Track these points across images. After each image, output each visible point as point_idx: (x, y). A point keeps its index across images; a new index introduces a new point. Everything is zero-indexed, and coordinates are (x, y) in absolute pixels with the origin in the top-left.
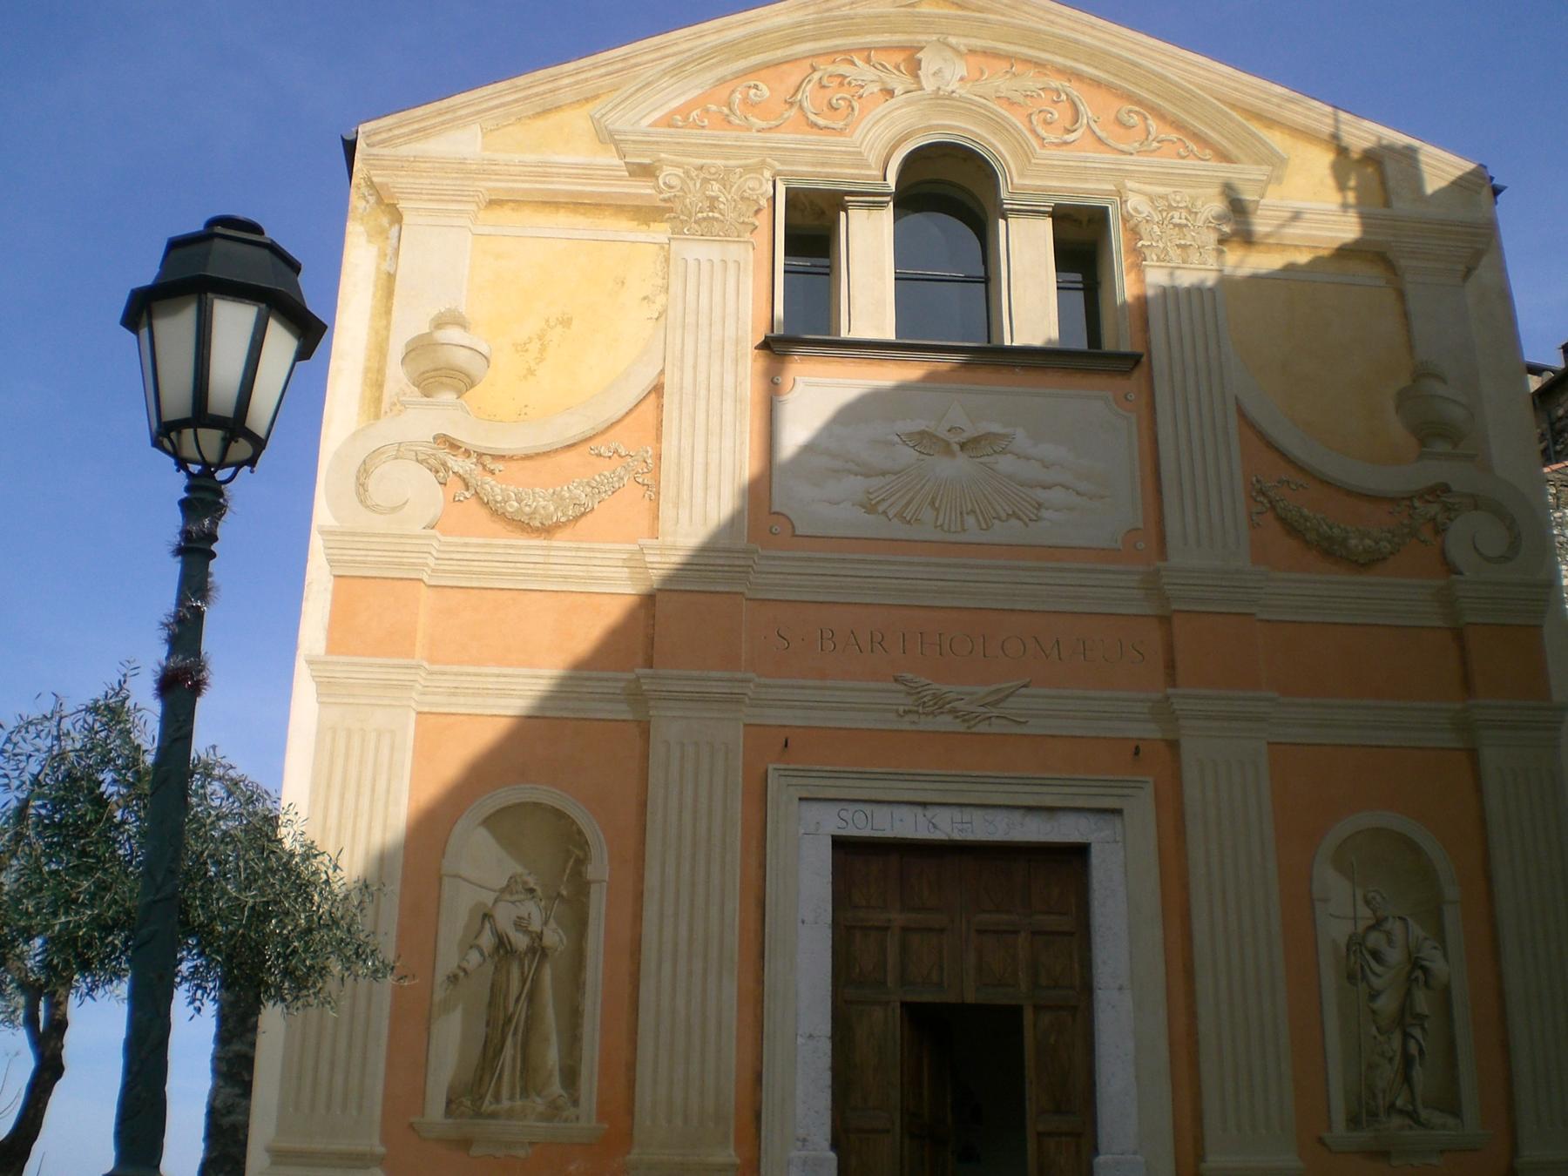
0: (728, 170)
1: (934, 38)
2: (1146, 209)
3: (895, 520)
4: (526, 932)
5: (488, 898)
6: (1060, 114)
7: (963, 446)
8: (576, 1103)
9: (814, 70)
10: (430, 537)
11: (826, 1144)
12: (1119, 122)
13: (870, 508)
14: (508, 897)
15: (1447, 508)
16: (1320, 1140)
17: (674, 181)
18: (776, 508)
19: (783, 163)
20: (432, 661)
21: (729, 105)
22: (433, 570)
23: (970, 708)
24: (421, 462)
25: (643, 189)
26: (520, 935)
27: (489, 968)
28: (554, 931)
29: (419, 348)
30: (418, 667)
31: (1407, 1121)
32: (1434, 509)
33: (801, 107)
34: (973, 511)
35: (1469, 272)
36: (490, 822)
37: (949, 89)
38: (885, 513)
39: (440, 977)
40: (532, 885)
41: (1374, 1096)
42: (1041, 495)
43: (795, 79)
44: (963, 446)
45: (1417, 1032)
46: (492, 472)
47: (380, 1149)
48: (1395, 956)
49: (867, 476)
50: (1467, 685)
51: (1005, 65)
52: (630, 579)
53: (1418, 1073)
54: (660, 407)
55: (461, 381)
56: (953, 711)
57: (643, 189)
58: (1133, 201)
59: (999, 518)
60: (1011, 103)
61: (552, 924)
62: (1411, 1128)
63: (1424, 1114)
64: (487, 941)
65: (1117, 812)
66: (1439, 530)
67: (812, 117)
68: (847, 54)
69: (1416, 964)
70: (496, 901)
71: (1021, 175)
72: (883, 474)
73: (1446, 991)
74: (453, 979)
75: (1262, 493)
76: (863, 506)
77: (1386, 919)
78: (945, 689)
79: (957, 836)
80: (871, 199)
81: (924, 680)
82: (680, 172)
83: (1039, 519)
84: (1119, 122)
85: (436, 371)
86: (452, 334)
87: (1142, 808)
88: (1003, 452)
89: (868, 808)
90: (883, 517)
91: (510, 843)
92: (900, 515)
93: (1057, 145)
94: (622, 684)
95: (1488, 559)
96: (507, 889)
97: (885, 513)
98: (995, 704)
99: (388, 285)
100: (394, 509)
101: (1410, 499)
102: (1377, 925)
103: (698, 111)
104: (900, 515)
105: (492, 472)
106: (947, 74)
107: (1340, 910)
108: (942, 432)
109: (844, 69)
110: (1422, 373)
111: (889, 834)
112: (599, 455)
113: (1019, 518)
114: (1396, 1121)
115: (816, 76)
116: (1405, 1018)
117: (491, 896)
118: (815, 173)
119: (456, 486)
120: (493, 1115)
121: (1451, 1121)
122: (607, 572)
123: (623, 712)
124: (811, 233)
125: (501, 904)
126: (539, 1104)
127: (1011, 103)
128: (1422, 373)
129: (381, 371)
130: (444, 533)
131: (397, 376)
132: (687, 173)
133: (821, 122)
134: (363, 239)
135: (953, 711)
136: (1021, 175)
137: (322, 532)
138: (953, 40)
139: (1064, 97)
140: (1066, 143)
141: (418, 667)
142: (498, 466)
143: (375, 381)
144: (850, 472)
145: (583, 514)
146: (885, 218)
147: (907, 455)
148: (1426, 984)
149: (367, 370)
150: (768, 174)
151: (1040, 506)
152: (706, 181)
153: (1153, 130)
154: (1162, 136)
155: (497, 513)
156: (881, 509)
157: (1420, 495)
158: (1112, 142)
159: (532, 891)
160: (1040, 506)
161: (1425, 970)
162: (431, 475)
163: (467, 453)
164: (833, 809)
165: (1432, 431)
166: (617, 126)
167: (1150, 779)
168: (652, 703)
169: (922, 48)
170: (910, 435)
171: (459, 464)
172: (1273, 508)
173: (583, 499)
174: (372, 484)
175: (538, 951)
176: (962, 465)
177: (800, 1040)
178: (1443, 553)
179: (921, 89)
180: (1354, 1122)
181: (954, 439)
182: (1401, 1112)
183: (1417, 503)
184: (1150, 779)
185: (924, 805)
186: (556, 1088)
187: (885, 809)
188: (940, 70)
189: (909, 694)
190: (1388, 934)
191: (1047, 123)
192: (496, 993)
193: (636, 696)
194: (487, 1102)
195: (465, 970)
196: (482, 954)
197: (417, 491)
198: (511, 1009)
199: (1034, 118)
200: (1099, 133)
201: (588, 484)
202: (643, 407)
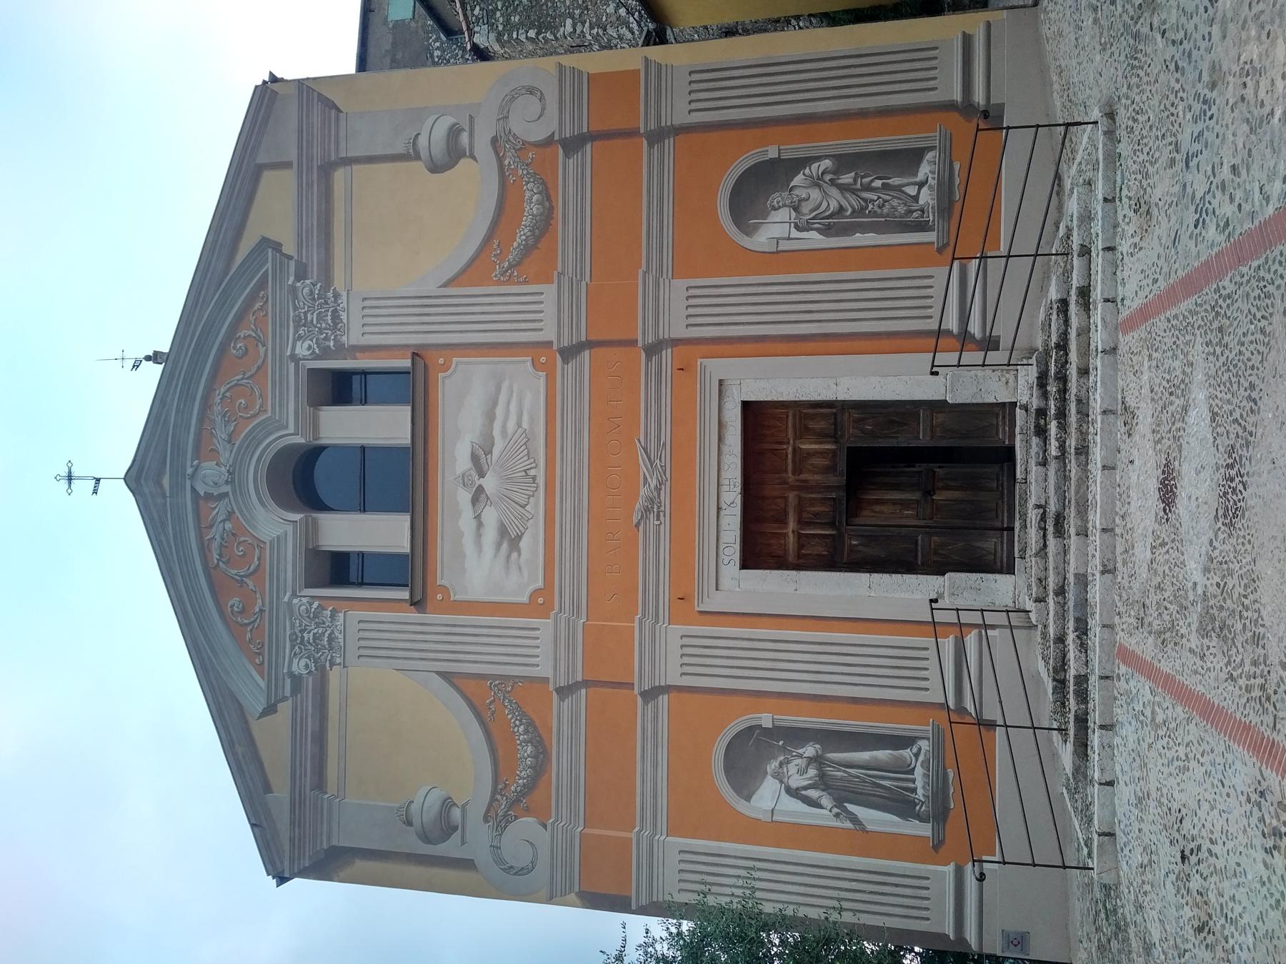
1: (188, 483)
11: (940, 578)
50: (632, 133)
56: (658, 490)
65: (721, 382)
67: (252, 567)
71: (286, 427)
79: (738, 489)
80: (311, 531)
82: (295, 661)
87: (716, 368)
89: (722, 546)
95: (543, 109)
109: (215, 545)
111: (738, 533)
146: (325, 519)
158: (260, 362)
164: (723, 568)
167: (699, 361)
175: (817, 760)
178: (537, 145)
184: (699, 361)
185: (719, 509)
186: (907, 753)
187: (722, 534)
193: (650, 695)
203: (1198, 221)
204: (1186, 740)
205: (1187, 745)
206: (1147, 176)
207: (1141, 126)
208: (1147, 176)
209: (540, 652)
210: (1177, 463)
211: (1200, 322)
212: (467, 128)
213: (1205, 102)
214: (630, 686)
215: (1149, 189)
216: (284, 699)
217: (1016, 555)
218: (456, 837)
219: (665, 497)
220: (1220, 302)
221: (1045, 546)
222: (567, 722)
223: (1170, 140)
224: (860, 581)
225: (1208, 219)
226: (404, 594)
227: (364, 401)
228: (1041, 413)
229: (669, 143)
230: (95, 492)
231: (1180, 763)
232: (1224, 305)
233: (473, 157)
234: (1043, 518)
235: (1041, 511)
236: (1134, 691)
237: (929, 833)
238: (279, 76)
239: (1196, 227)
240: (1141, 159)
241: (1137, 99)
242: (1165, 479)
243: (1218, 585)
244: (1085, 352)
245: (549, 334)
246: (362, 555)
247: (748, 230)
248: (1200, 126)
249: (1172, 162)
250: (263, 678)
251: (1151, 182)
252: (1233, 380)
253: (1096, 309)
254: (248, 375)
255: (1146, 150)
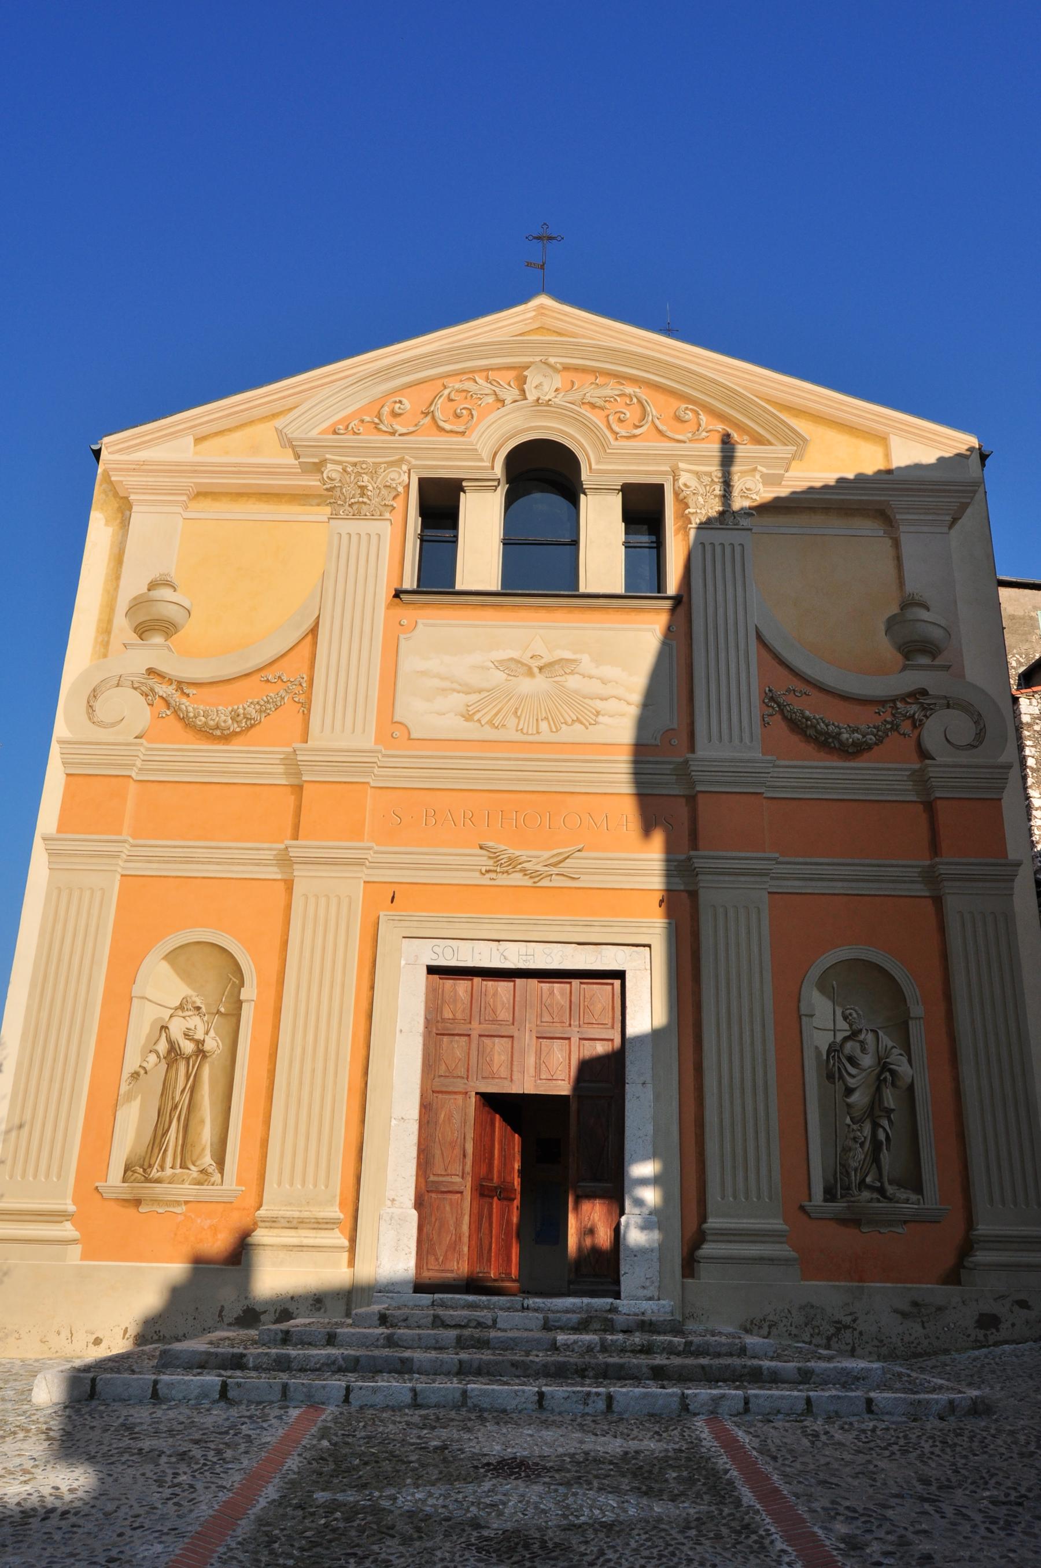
0: (377, 465)
1: (538, 359)
2: (693, 483)
3: (487, 726)
4: (192, 1040)
5: (166, 1014)
6: (631, 414)
7: (541, 669)
8: (221, 1171)
9: (445, 387)
10: (136, 744)
12: (678, 419)
13: (468, 717)
14: (180, 1013)
15: (924, 708)
16: (802, 1208)
17: (334, 475)
18: (395, 720)
19: (415, 458)
20: (134, 838)
21: (379, 416)
22: (140, 769)
23: (539, 867)
24: (135, 689)
25: (312, 482)
26: (188, 1042)
27: (163, 1066)
28: (213, 1039)
29: (138, 604)
30: (125, 841)
31: (875, 1195)
32: (913, 709)
33: (433, 418)
34: (546, 718)
35: (955, 521)
36: (171, 957)
37: (547, 398)
38: (479, 721)
39: (126, 1075)
40: (199, 1004)
41: (848, 1174)
42: (599, 705)
43: (429, 396)
44: (541, 669)
45: (885, 1123)
46: (188, 695)
47: (72, 1208)
48: (867, 1061)
49: (467, 693)
50: (935, 847)
51: (591, 378)
52: (285, 774)
53: (885, 1156)
54: (315, 644)
55: (167, 628)
56: (524, 871)
57: (312, 482)
58: (684, 478)
59: (566, 723)
60: (593, 406)
61: (212, 1033)
62: (879, 1201)
63: (890, 1189)
64: (162, 1047)
66: (917, 724)
67: (442, 424)
68: (470, 373)
69: (884, 1066)
70: (171, 1016)
71: (598, 462)
72: (480, 691)
73: (911, 1088)
74: (135, 1075)
75: (772, 699)
76: (463, 716)
77: (861, 1031)
78: (518, 853)
80: (484, 484)
81: (504, 847)
82: (339, 468)
83: (596, 723)
84: (678, 419)
85: (151, 624)
86: (166, 593)
88: (572, 673)
90: (477, 724)
91: (185, 975)
92: (490, 722)
93: (628, 438)
94: (275, 852)
95: (958, 747)
96: (181, 1007)
97: (479, 721)
98: (555, 865)
99: (118, 559)
100: (113, 725)
101: (894, 701)
102: (854, 1035)
103: (356, 422)
104: (490, 722)
105: (188, 695)
106: (546, 388)
107: (824, 1020)
108: (526, 659)
109: (469, 385)
110: (909, 603)
112: (268, 681)
113: (581, 723)
114: (866, 1195)
115: (446, 392)
116: (875, 1110)
117: (166, 1014)
118: (444, 469)
119: (157, 701)
120: (158, 1181)
121: (914, 1197)
122: (269, 769)
123: (273, 873)
124: (440, 507)
125: (174, 1019)
126: (194, 1172)
127: (593, 406)
128: (909, 603)
129: (110, 621)
130: (150, 741)
131: (121, 623)
132: (345, 470)
133: (447, 426)
134: (103, 522)
135: (524, 871)
136: (598, 462)
137: (59, 742)
138: (552, 360)
139: (635, 400)
140: (635, 436)
141: (125, 841)
142: (190, 691)
143: (106, 629)
144: (454, 690)
145: (252, 726)
147: (499, 676)
148: (893, 1084)
149: (100, 620)
150: (405, 468)
151: (598, 713)
152: (359, 474)
153: (703, 424)
154: (711, 427)
155: (186, 722)
156: (476, 718)
157: (903, 698)
159: (198, 1008)
160: (598, 713)
161: (893, 1072)
162: (142, 699)
163: (170, 681)
165: (916, 648)
166: (295, 435)
168: (296, 866)
169: (528, 368)
170: (501, 662)
171: (163, 689)
172: (781, 711)
173: (254, 714)
174: (97, 705)
175: (201, 1052)
176: (540, 683)
177: (394, 1122)
178: (919, 745)
179: (526, 399)
180: (830, 1194)
181: (535, 664)
182: (870, 1188)
183: (899, 705)
186: (208, 1160)
188: (541, 384)
189: (490, 858)
190: (862, 1043)
191: (620, 421)
192: (166, 1087)
193: (285, 861)
194: (155, 1170)
195: (144, 1068)
196: (158, 1057)
197: (132, 711)
198: (177, 1099)
199: (611, 418)
200: (661, 427)
201: (258, 703)
202: (300, 647)
203: (855, 1511)
204: (199, 1486)
205: (191, 1486)
206: (904, 1452)
207: (966, 1445)
208: (904, 1452)
209: (340, 728)
210: (547, 1480)
211: (726, 1511)
212: (936, 663)
213: (1008, 1523)
214: (296, 837)
215: (887, 1453)
216: (297, 456)
217: (436, 1296)
218: (134, 638)
219: (517, 879)
220: (754, 1537)
221: (446, 1326)
222: (256, 761)
223: (953, 1480)
224: (411, 1110)
225: (859, 1523)
226: (410, 582)
227: (627, 545)
228: (609, 1326)
229: (920, 889)
230: (529, 265)
231: (169, 1478)
232: (750, 1542)
233: (905, 668)
234: (480, 1325)
235: (490, 1323)
236: (265, 1425)
237: (110, 1183)
238: (987, 462)
239: (848, 1508)
240: (923, 1443)
241: (999, 1442)
242: (528, 1467)
243: (393, 1527)
244: (683, 1377)
245: (704, 750)
246: (455, 541)
247: (822, 986)
248: (978, 1518)
249: (926, 1481)
250: (319, 434)
251: (898, 1455)
252: (655, 1551)
253: (737, 1388)
254: (657, 422)
255: (937, 1451)
